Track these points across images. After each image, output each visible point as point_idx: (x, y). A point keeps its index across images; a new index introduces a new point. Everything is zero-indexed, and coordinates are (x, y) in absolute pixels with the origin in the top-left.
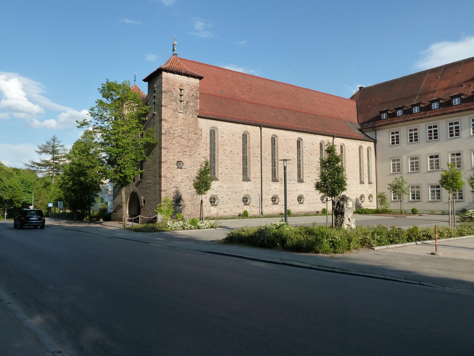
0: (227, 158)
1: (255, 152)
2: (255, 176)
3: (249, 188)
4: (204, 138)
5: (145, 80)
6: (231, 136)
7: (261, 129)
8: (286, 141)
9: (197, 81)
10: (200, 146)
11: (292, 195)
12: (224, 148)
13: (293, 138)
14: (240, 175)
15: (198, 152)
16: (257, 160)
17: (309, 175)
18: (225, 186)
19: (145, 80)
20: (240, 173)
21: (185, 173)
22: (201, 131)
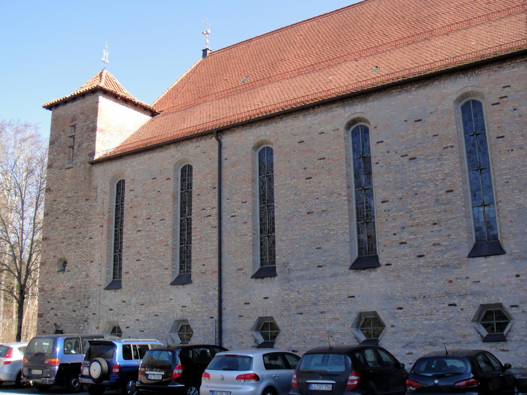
0: (139, 234)
1: (203, 206)
2: (203, 269)
3: (187, 301)
4: (100, 202)
5: (50, 107)
6: (150, 181)
7: (144, 109)
8: (302, 146)
9: (146, 118)
10: (93, 220)
11: (329, 316)
12: (135, 214)
13: (328, 128)
14: (166, 272)
15: (89, 235)
16: (209, 224)
17: (405, 236)
18: (134, 300)
19: (50, 107)
20: (166, 265)
21: (69, 281)
22: (96, 192)
